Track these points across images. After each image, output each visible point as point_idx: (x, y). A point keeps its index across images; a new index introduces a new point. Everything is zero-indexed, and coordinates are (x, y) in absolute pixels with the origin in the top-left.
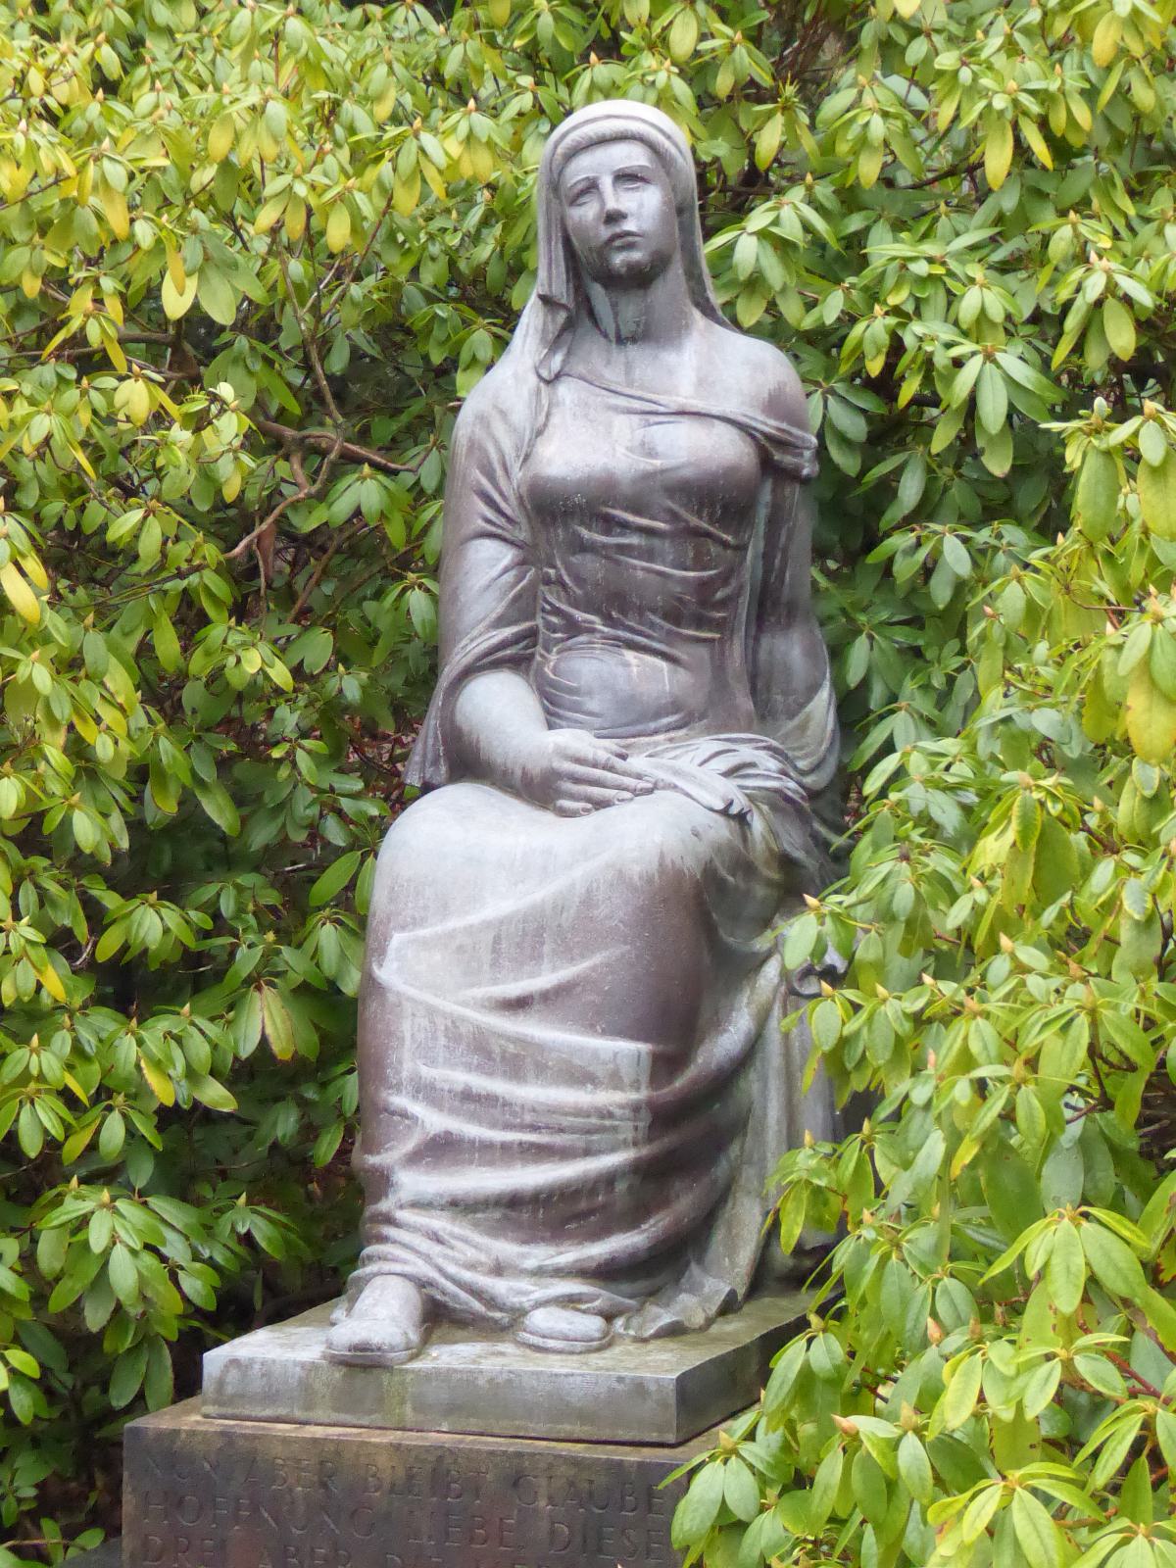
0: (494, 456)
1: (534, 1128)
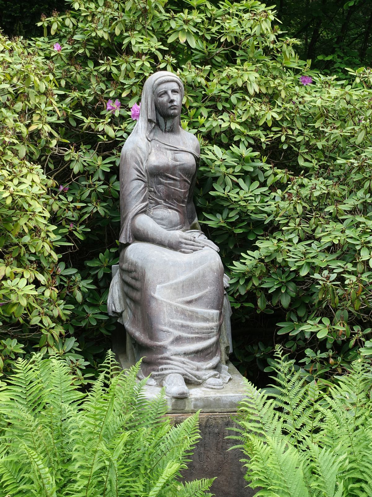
0: (139, 160)
1: (198, 333)
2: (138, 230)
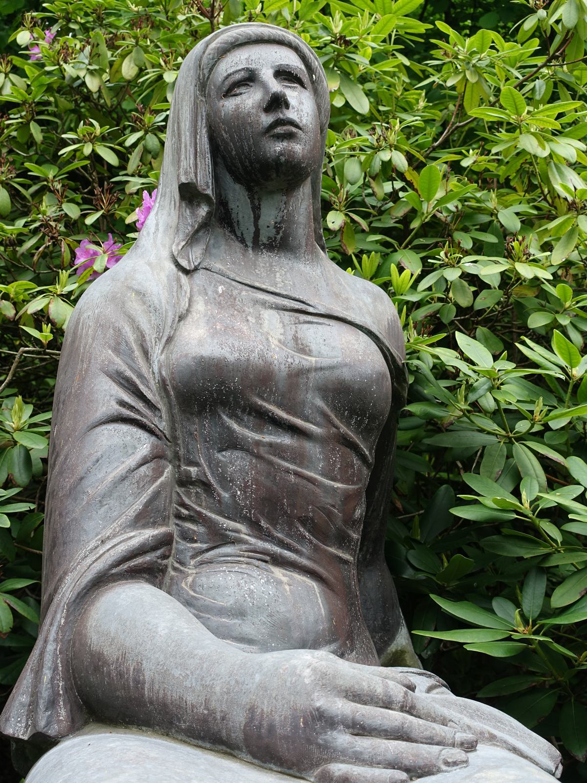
0: (131, 337)
2: (98, 661)
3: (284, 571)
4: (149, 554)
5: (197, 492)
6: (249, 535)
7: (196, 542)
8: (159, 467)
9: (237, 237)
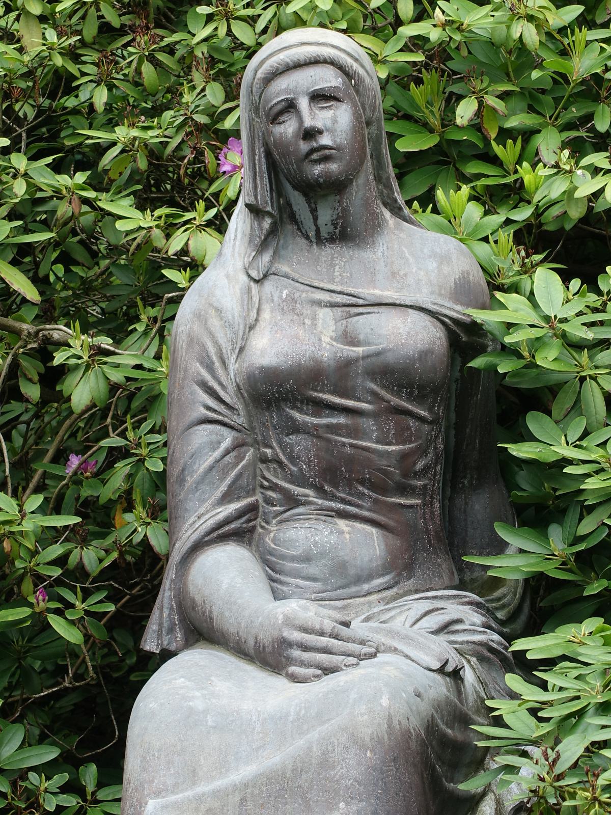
0: (212, 351)
3: (348, 522)
4: (234, 523)
5: (274, 468)
6: (316, 498)
7: (276, 506)
8: (240, 454)
9: (303, 234)
